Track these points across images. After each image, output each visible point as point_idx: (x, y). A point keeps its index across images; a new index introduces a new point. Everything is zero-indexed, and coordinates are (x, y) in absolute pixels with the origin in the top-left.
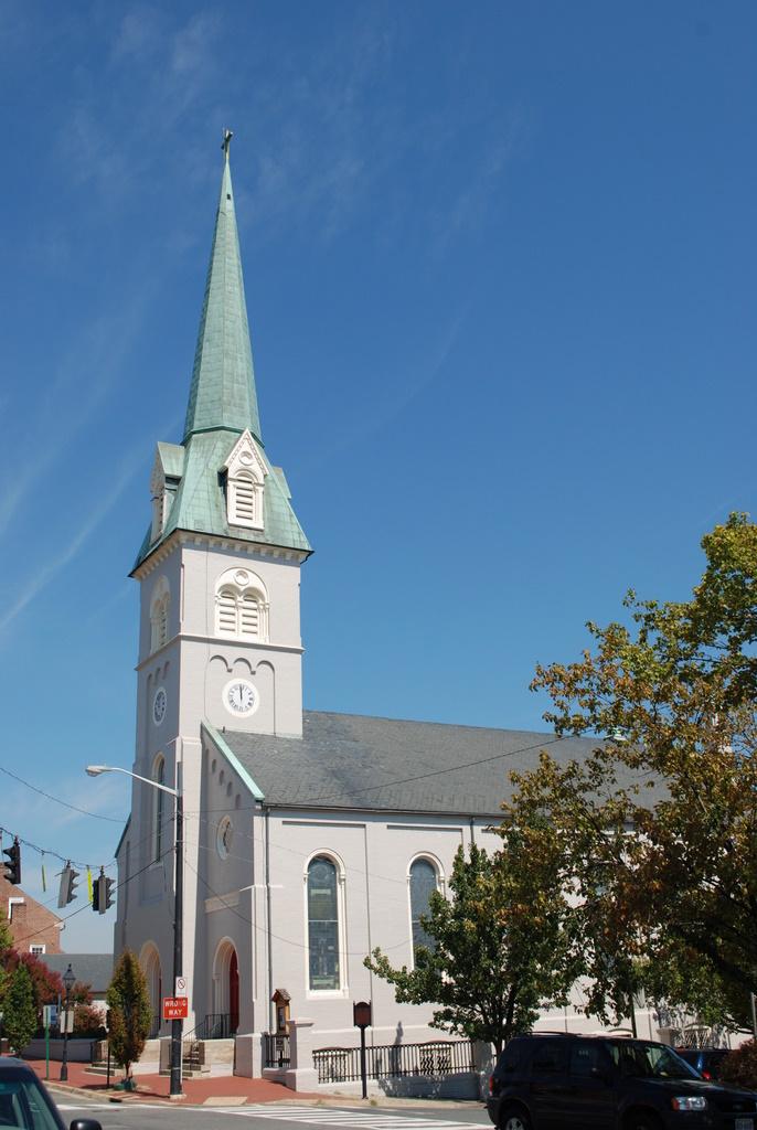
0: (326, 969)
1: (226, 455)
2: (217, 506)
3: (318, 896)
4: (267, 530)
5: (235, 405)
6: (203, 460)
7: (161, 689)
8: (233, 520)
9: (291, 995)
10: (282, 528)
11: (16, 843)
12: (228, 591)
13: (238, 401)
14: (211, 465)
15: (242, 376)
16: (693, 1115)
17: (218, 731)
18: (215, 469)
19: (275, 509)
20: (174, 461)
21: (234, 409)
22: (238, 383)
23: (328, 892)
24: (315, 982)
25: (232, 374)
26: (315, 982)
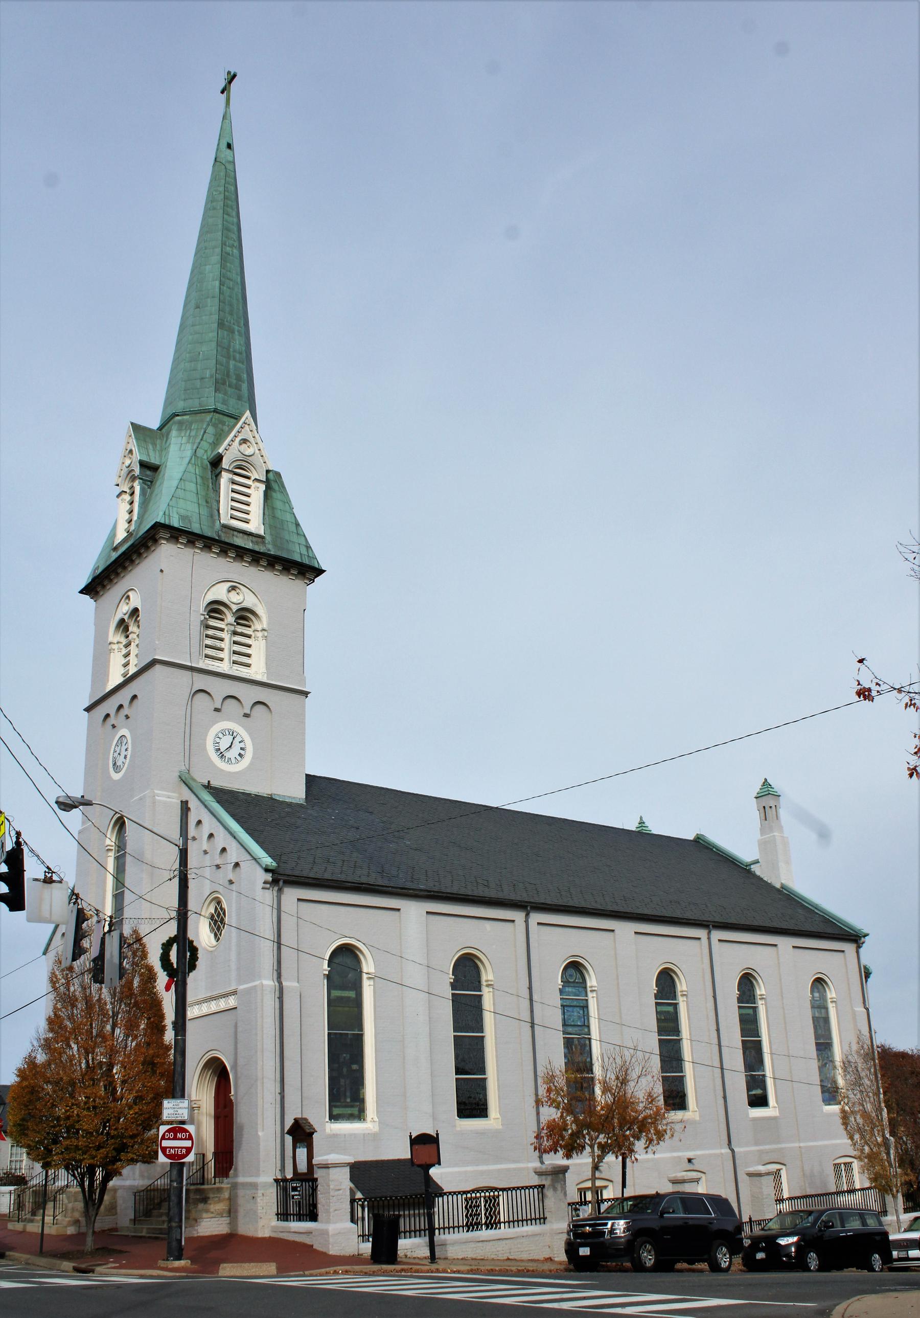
0: (348, 1094)
1: (219, 438)
2: (207, 502)
3: (340, 999)
4: (268, 538)
5: (230, 386)
6: (189, 446)
7: (124, 731)
8: (225, 519)
9: (316, 1126)
10: (287, 537)
11: (18, 843)
12: (215, 609)
13: (234, 381)
14: (200, 452)
15: (241, 353)
16: (762, 1260)
17: (204, 786)
18: (206, 455)
19: (278, 514)
20: (150, 447)
21: (230, 391)
22: (235, 359)
23: (352, 994)
24: (336, 1111)
25: (228, 349)
26: (336, 1111)
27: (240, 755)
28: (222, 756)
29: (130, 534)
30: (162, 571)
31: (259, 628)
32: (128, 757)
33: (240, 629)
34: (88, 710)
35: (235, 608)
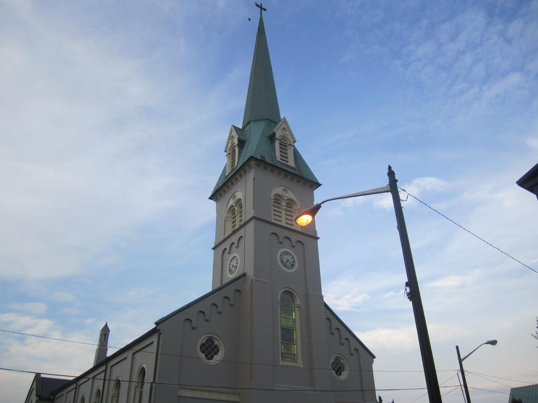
27: (292, 265)
28: (285, 265)
29: (232, 170)
30: (250, 20)
31: (296, 208)
32: (238, 267)
33: (289, 209)
34: (213, 249)
35: (286, 198)
